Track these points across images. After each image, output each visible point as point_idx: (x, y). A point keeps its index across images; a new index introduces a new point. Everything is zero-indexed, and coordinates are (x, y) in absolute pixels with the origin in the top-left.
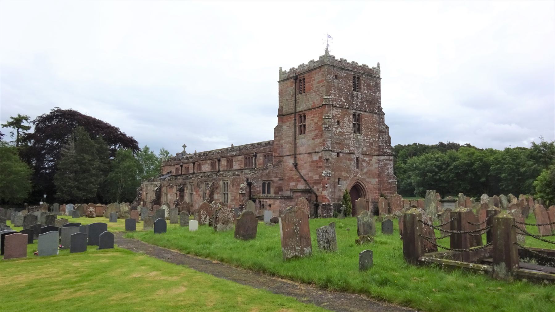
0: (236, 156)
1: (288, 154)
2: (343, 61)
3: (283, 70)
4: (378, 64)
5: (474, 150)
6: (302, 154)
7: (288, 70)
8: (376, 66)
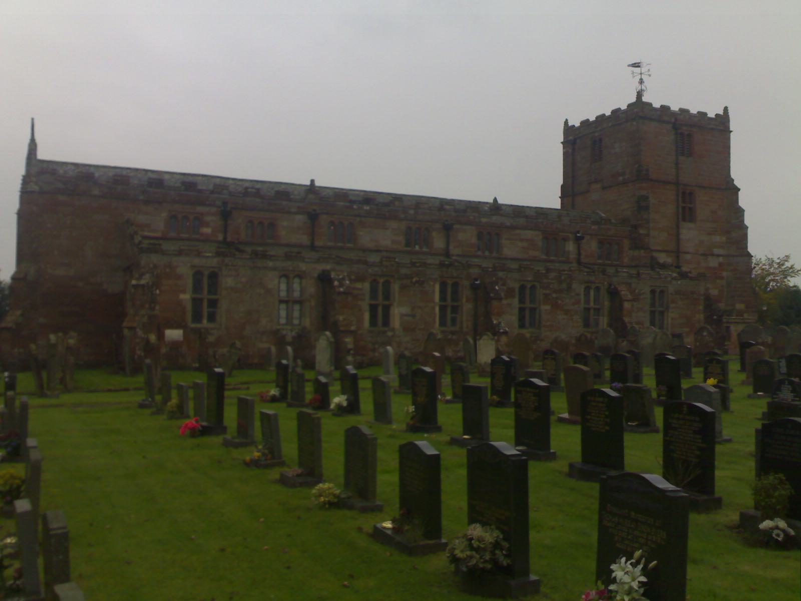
0: (513, 228)
1: (659, 248)
2: (665, 109)
3: (570, 124)
4: (726, 109)
5: (231, 182)
6: (688, 253)
7: (577, 124)
8: (721, 112)
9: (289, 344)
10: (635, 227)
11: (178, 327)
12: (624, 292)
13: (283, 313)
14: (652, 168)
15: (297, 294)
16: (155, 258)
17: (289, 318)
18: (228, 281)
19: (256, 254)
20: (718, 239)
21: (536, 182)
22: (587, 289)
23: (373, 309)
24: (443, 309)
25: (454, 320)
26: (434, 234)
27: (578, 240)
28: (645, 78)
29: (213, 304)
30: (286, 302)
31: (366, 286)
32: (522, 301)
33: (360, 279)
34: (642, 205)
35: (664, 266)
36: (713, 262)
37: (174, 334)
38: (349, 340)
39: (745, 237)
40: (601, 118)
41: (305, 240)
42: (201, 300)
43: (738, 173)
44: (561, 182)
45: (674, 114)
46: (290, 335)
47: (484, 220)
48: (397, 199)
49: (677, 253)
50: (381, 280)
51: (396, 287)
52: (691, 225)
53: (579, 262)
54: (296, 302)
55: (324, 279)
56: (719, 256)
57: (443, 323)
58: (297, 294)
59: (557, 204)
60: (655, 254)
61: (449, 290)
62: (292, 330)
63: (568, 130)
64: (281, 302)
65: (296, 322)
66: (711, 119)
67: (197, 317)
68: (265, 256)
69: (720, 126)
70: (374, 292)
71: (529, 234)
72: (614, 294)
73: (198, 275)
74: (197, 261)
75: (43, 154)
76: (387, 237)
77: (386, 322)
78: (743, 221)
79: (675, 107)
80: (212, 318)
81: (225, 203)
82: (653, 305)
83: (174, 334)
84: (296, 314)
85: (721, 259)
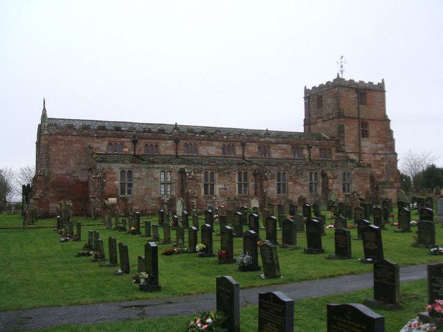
2: (351, 81)
4: (383, 80)
9: (166, 204)
10: (338, 141)
11: (116, 197)
12: (329, 175)
13: (163, 189)
14: (349, 112)
15: (169, 180)
16: (104, 165)
17: (166, 191)
18: (136, 175)
19: (149, 161)
20: (380, 146)
21: (288, 117)
22: (311, 174)
23: (206, 186)
24: (240, 185)
25: (245, 192)
26: (236, 148)
27: (309, 148)
28: (344, 65)
29: (130, 185)
30: (164, 184)
31: (203, 175)
32: (279, 180)
33: (200, 172)
34: (341, 130)
35: (352, 161)
36: (378, 158)
37: (113, 200)
38: (194, 201)
39: (394, 144)
40: (321, 86)
41: (173, 153)
42: (124, 184)
43: (390, 112)
44: (304, 118)
45: (356, 84)
46: (166, 199)
47: (261, 140)
48: (218, 130)
49: (360, 153)
50: (209, 172)
51: (216, 175)
52: (366, 139)
53: (310, 159)
54: (168, 184)
55: (182, 172)
56: (381, 154)
57: (240, 192)
58: (169, 180)
59: (301, 129)
60: (348, 155)
61: (243, 176)
62: (167, 197)
63: (306, 91)
64: (162, 184)
65: (169, 193)
66: (375, 85)
67: (123, 192)
68: (154, 163)
69: (380, 89)
70: (206, 179)
71: (284, 146)
72: (324, 175)
73: (123, 172)
74: (122, 165)
75: (49, 116)
76: (213, 150)
77: (212, 193)
78: (392, 136)
79: (357, 80)
80: (129, 192)
81: (134, 136)
82: (344, 180)
83: (113, 200)
84: (169, 189)
85: (382, 156)
